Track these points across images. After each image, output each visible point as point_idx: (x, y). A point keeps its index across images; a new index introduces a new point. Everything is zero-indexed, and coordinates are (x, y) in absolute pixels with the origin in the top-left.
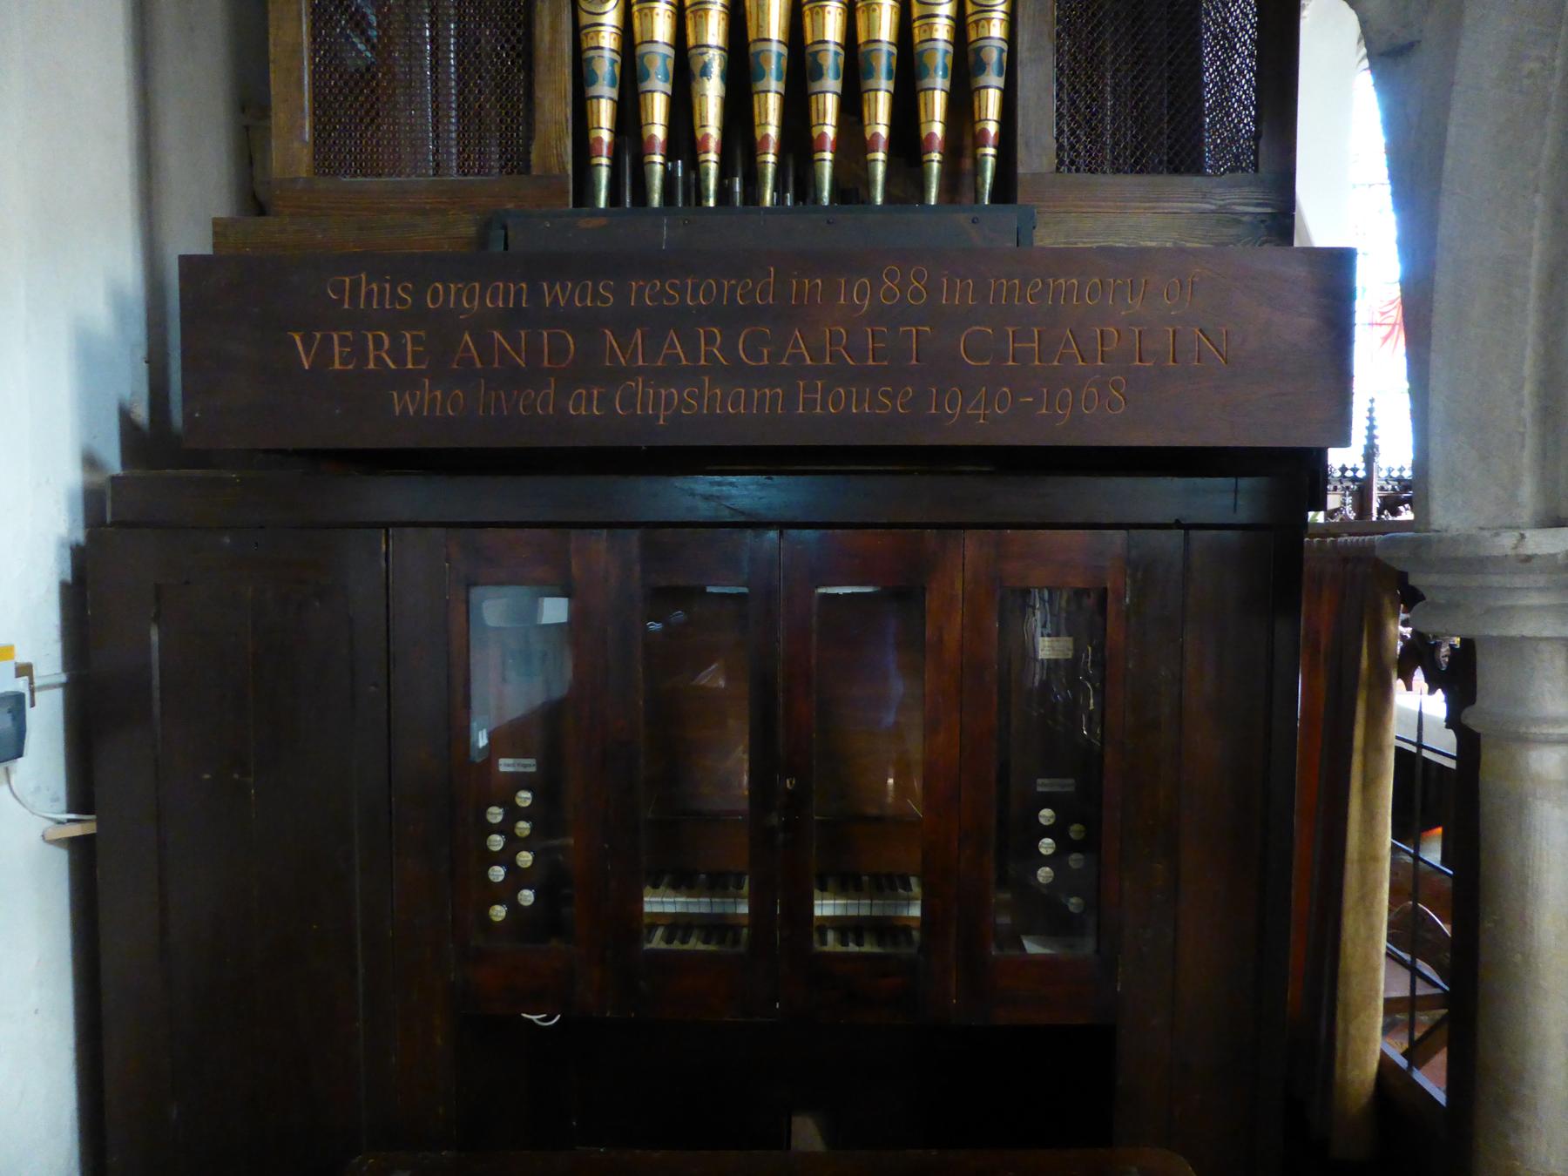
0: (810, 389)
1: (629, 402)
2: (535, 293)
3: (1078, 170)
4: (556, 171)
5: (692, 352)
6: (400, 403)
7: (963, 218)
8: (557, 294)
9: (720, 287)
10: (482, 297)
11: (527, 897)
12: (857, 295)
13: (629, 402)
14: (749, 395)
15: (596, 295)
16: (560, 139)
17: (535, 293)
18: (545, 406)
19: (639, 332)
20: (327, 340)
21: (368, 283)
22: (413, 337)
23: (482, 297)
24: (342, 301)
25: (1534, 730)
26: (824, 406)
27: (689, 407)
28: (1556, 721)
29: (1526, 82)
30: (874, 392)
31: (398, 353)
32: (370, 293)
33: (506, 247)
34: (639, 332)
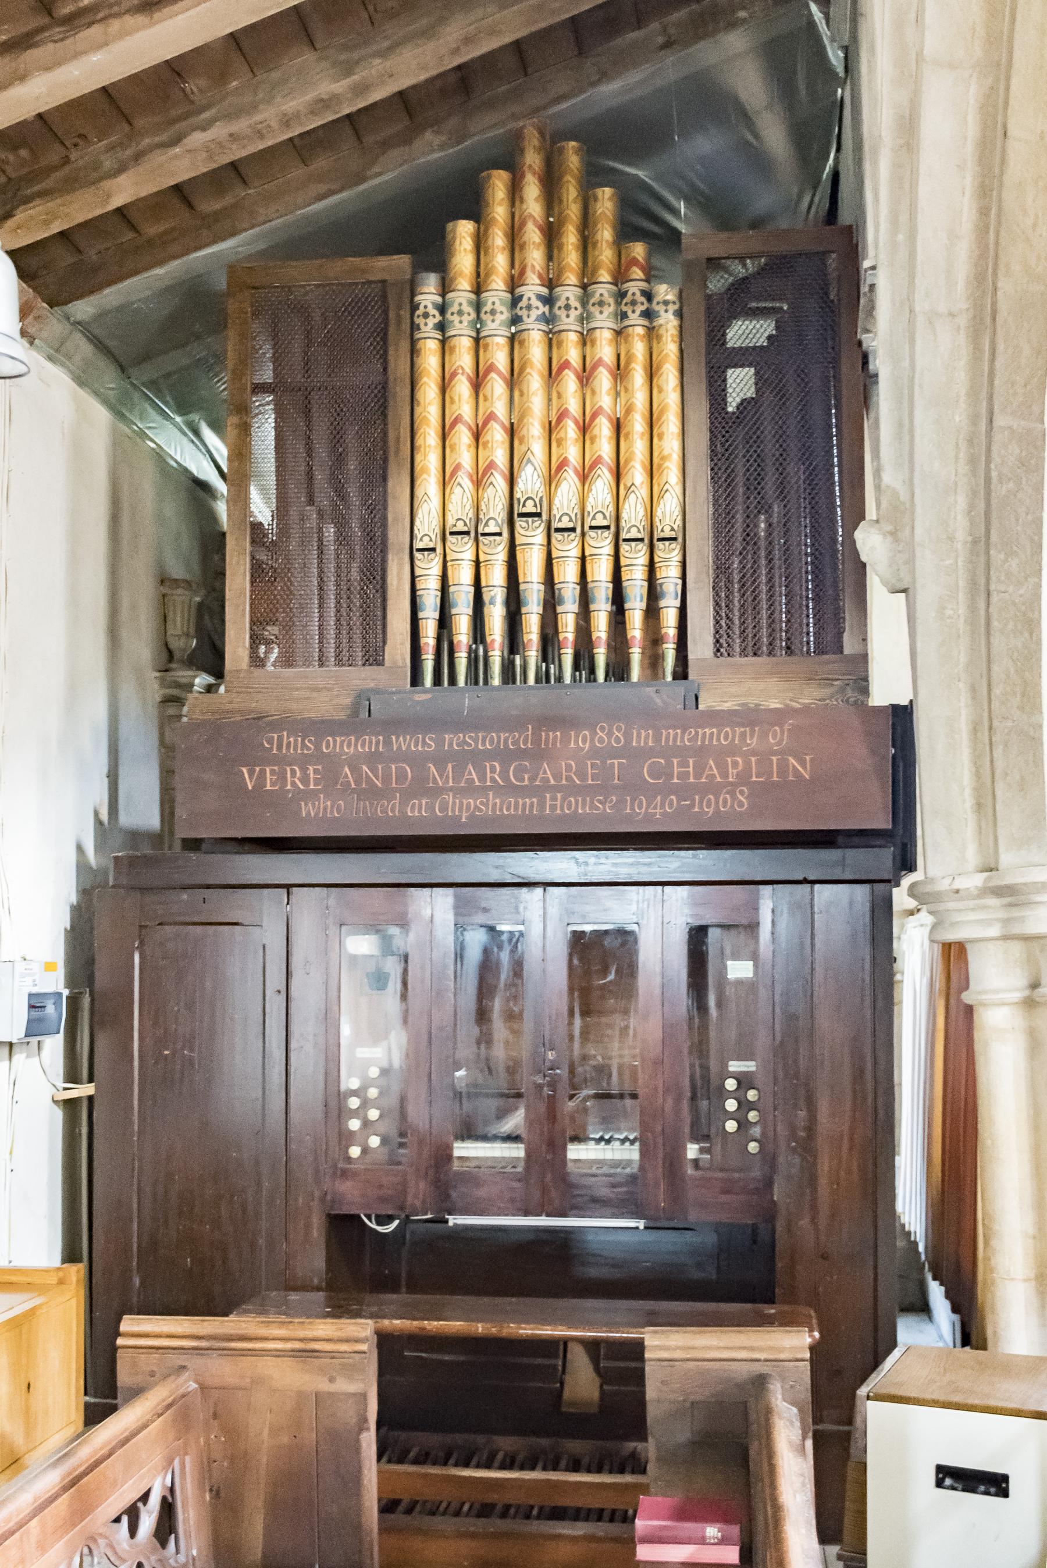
0: (554, 799)
1: (444, 808)
2: (388, 743)
3: (721, 655)
4: (400, 664)
5: (482, 778)
6: (307, 809)
7: (650, 691)
8: (401, 743)
9: (499, 738)
10: (356, 746)
11: (374, 1141)
12: (581, 741)
13: (444, 808)
14: (516, 803)
15: (424, 743)
16: (402, 644)
17: (388, 743)
18: (393, 811)
19: (450, 765)
20: (263, 772)
21: (288, 738)
22: (314, 770)
23: (356, 746)
24: (271, 749)
25: (984, 997)
26: (562, 809)
27: (480, 810)
28: (996, 991)
29: (948, 621)
30: (592, 801)
31: (305, 780)
32: (289, 743)
33: (369, 715)
34: (450, 765)
